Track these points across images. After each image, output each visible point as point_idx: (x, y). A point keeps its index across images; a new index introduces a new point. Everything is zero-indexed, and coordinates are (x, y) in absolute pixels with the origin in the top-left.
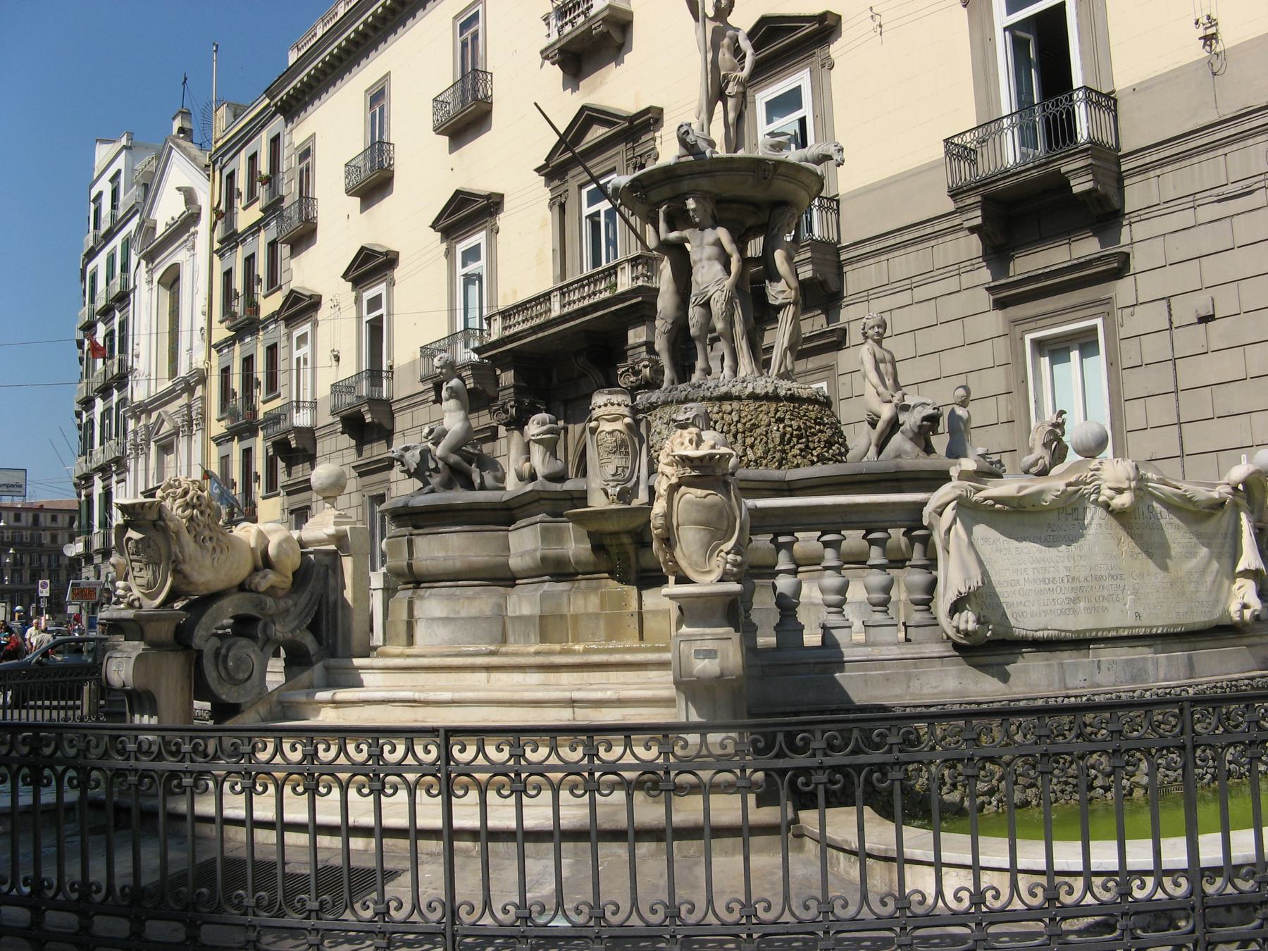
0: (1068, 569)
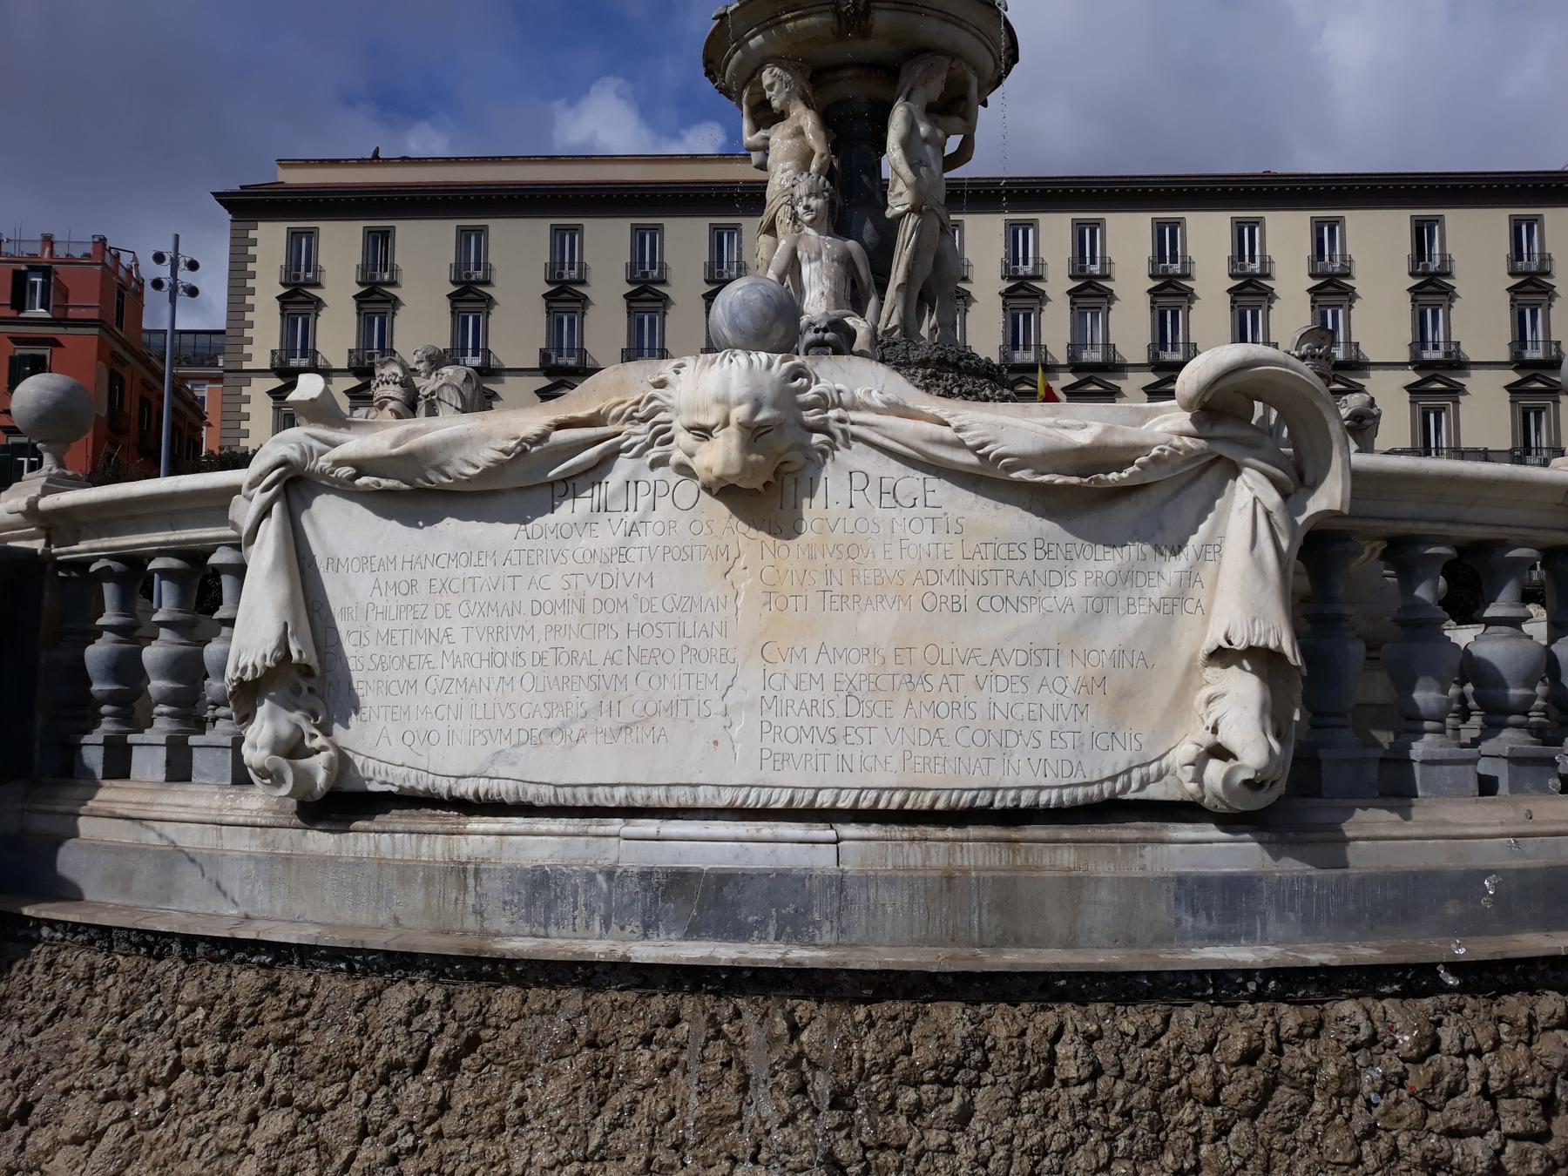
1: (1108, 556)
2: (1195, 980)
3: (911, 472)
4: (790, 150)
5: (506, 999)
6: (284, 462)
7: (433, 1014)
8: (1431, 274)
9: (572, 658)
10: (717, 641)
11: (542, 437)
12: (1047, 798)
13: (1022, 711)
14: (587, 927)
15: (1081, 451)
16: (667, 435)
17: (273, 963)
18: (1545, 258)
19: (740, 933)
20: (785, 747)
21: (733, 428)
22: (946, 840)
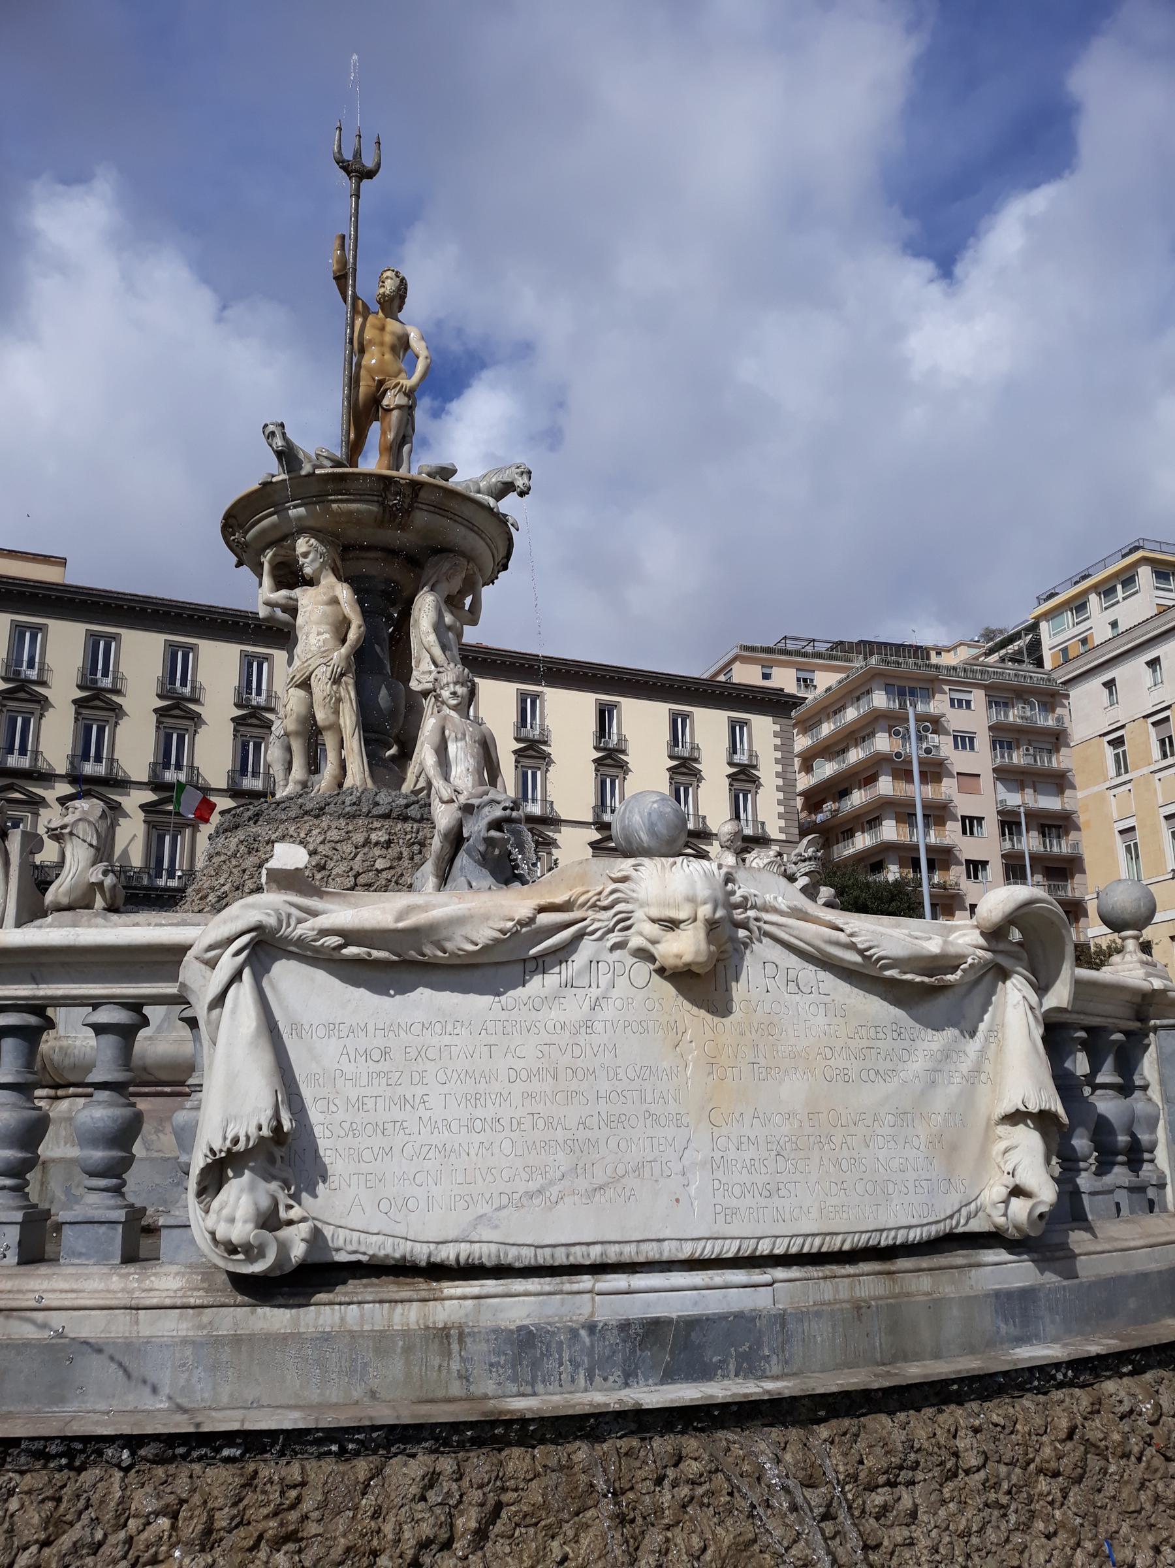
1: (935, 1038)
2: (1027, 1374)
3: (806, 965)
4: (324, 613)
5: (516, 1460)
6: (258, 928)
7: (446, 1485)
8: (610, 749)
9: (549, 1124)
10: (672, 1107)
11: (532, 920)
12: (915, 1235)
13: (895, 1164)
14: (573, 1381)
15: (934, 958)
17: (243, 1455)
18: (695, 748)
19: (705, 1373)
20: (734, 1203)
21: (700, 924)
22: (849, 1276)
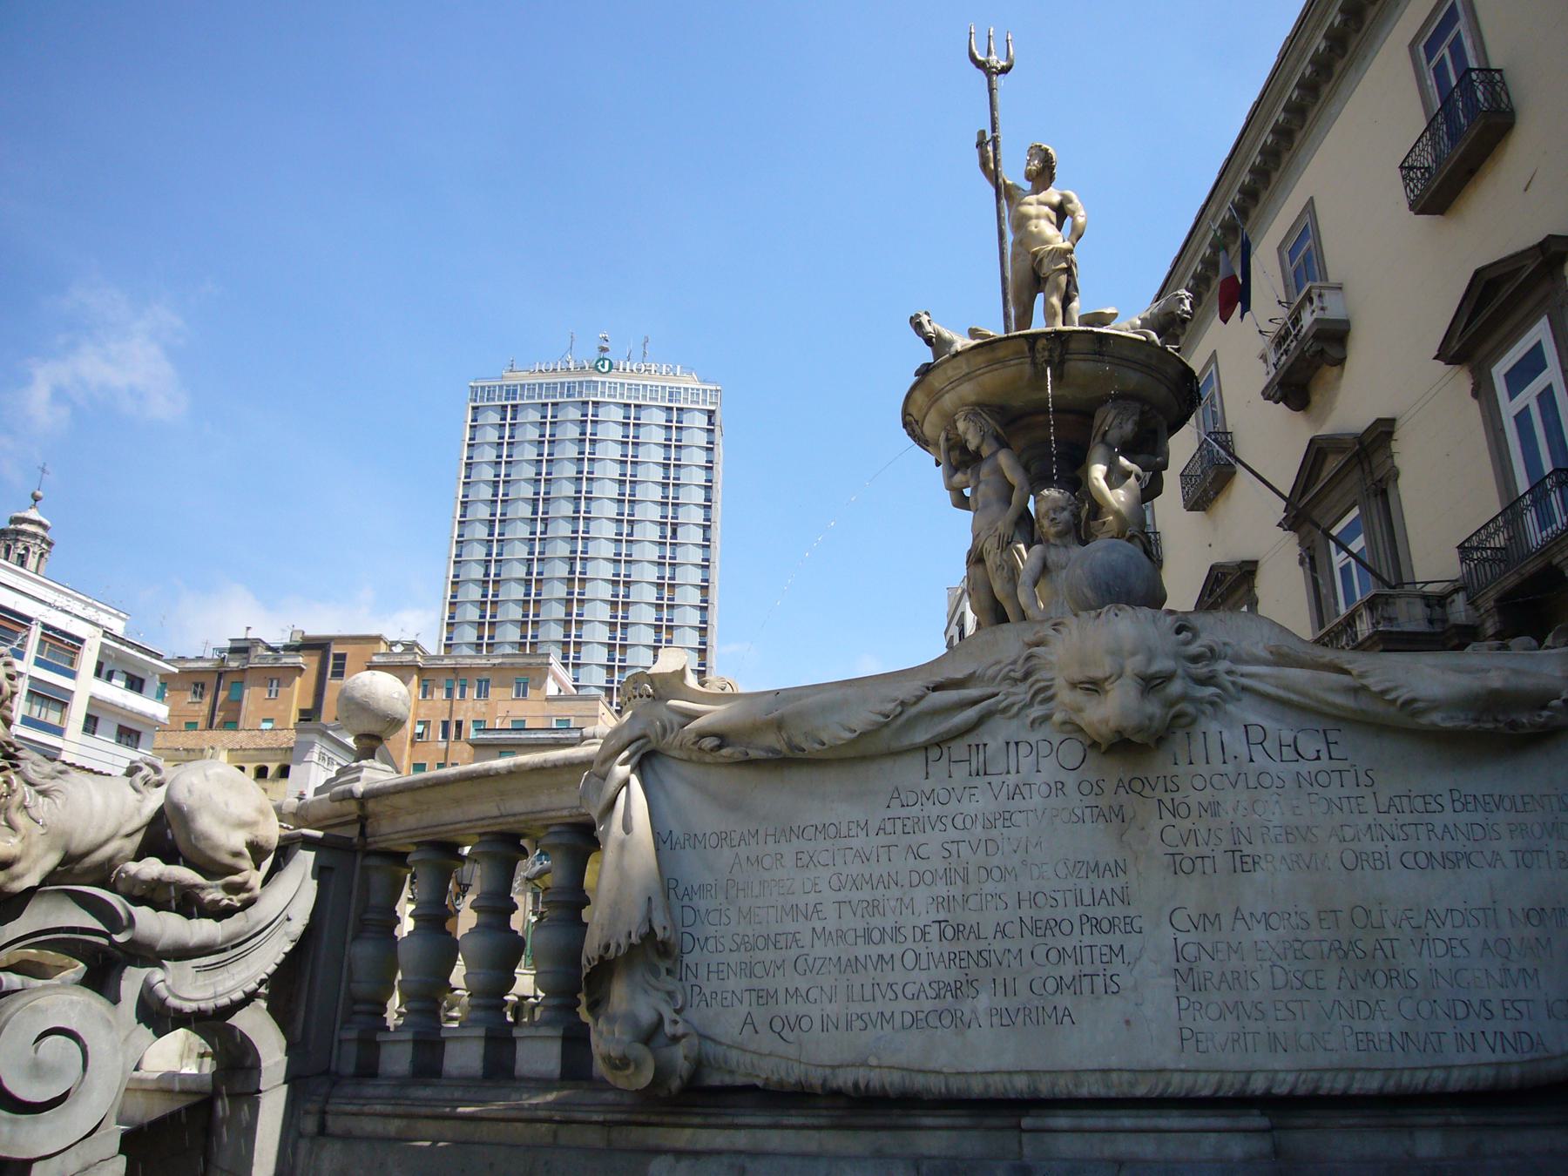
0: (944, 902)
16: (1049, 693)
